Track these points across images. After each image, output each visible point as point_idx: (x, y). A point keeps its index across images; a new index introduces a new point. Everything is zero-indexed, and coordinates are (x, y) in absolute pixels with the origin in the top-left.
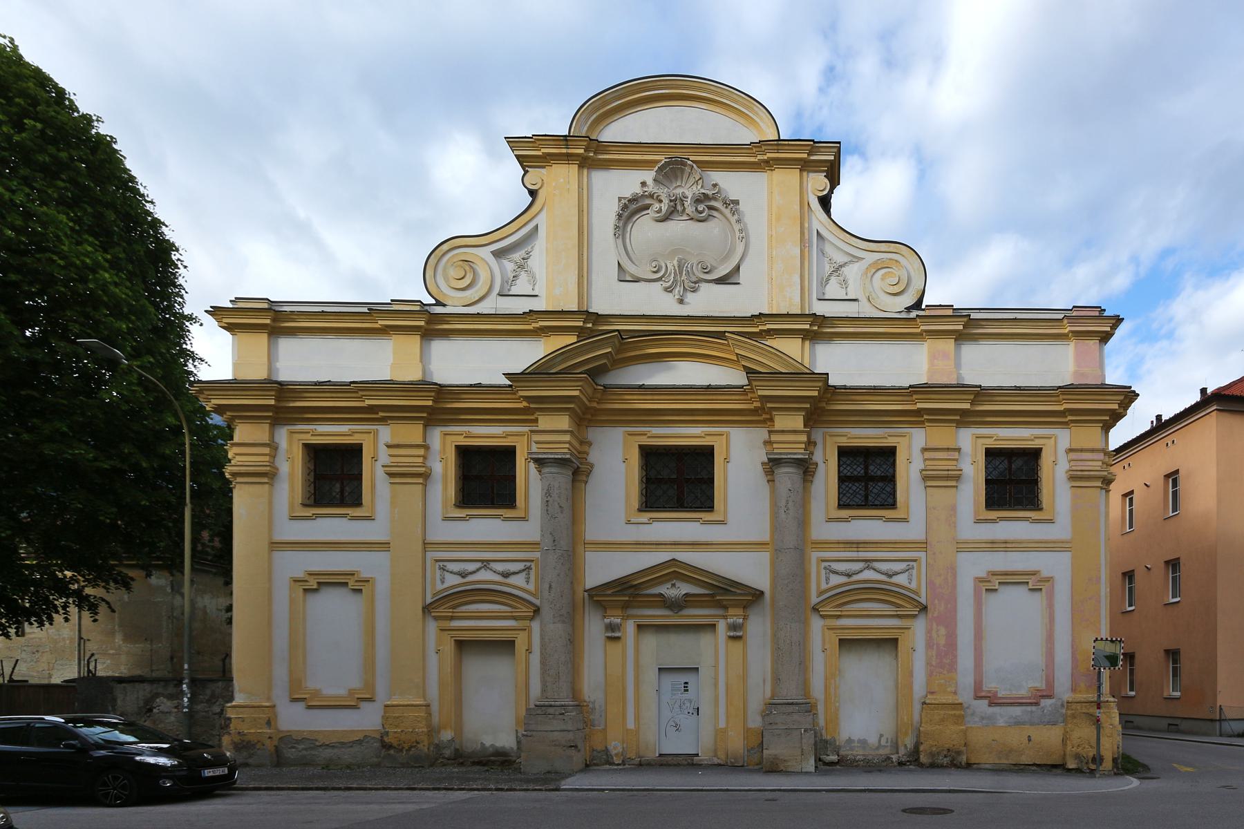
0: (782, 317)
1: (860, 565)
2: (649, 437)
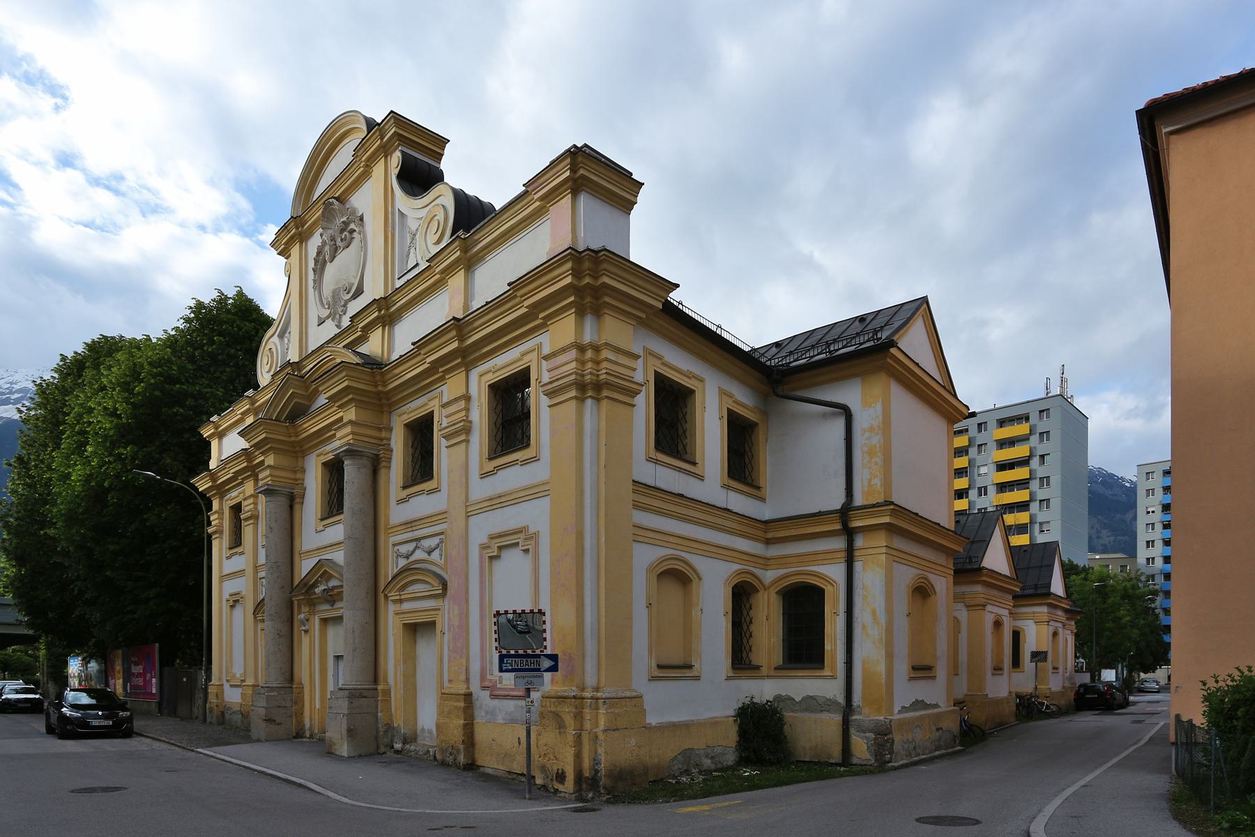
0: (366, 310)
1: (411, 546)
2: (325, 455)
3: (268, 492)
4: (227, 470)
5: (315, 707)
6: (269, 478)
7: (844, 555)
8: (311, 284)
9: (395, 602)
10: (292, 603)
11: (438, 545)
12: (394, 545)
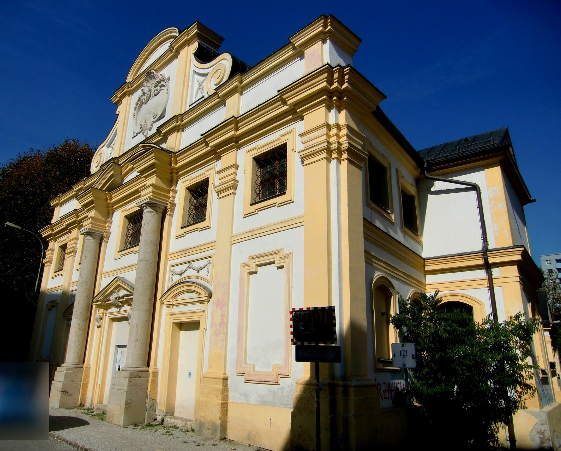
1: (185, 267)
3: (88, 233)
4: (63, 223)
5: (97, 383)
6: (90, 225)
7: (486, 282)
8: (131, 115)
9: (167, 306)
10: (92, 306)
11: (206, 265)
12: (172, 266)
